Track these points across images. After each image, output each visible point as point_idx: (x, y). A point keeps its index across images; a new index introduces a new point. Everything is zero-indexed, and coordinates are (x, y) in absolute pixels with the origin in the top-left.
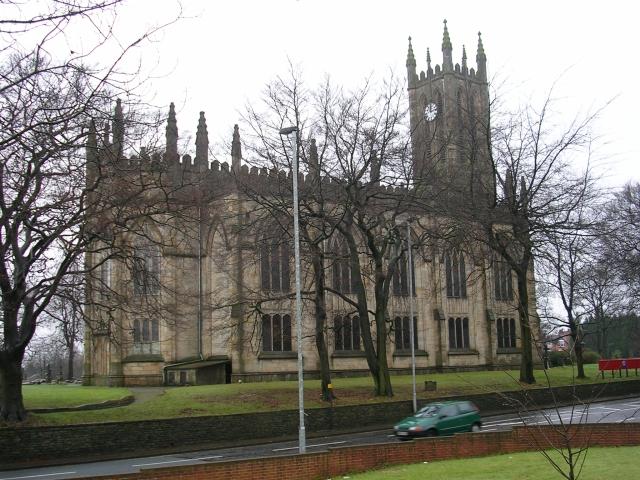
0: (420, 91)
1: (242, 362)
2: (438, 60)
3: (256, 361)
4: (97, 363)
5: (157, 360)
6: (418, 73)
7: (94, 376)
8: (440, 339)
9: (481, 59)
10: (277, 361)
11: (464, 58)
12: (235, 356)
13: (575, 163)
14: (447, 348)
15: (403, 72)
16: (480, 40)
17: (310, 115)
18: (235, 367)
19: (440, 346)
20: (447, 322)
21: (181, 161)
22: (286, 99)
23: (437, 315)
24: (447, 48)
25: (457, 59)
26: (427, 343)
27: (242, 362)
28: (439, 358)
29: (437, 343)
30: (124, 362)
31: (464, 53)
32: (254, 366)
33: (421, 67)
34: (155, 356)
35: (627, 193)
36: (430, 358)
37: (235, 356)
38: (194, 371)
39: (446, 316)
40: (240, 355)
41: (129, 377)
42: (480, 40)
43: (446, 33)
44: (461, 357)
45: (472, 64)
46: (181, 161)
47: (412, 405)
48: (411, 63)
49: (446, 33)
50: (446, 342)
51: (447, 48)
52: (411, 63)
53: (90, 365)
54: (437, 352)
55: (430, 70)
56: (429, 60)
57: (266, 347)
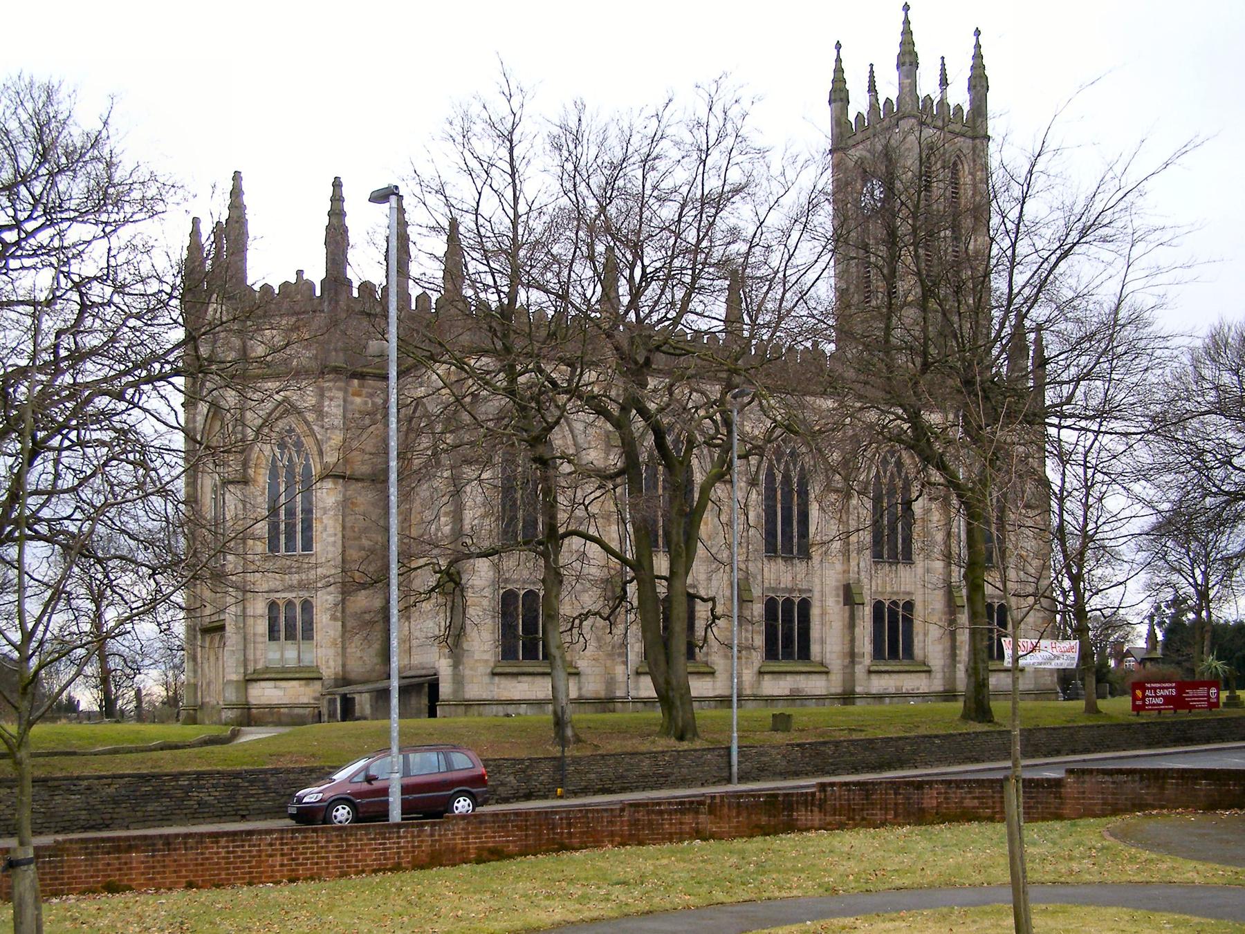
0: (856, 153)
1: (458, 680)
2: (889, 89)
3: (486, 679)
4: (209, 684)
5: (309, 676)
6: (852, 117)
7: (202, 706)
8: (852, 640)
9: (978, 82)
10: (529, 679)
11: (944, 82)
12: (444, 667)
13: (1091, 277)
14: (867, 660)
15: (824, 116)
16: (978, 46)
17: (543, 186)
18: (445, 689)
19: (852, 656)
20: (868, 611)
21: (355, 294)
22: (487, 147)
23: (849, 596)
24: (908, 60)
25: (927, 85)
26: (828, 648)
27: (458, 680)
28: (850, 677)
29: (847, 649)
30: (248, 681)
31: (942, 79)
32: (477, 688)
33: (859, 104)
34: (308, 668)
35: (1216, 346)
36: (833, 677)
37: (444, 667)
38: (367, 695)
39: (867, 599)
40: (456, 665)
41: (260, 707)
42: (907, 22)
43: (907, 32)
44: (895, 676)
45: (959, 95)
46: (355, 294)
47: (729, 755)
48: (839, 95)
49: (907, 32)
50: (865, 646)
51: (908, 60)
52: (839, 95)
53: (195, 685)
54: (845, 667)
55: (873, 106)
56: (872, 88)
57: (508, 653)
